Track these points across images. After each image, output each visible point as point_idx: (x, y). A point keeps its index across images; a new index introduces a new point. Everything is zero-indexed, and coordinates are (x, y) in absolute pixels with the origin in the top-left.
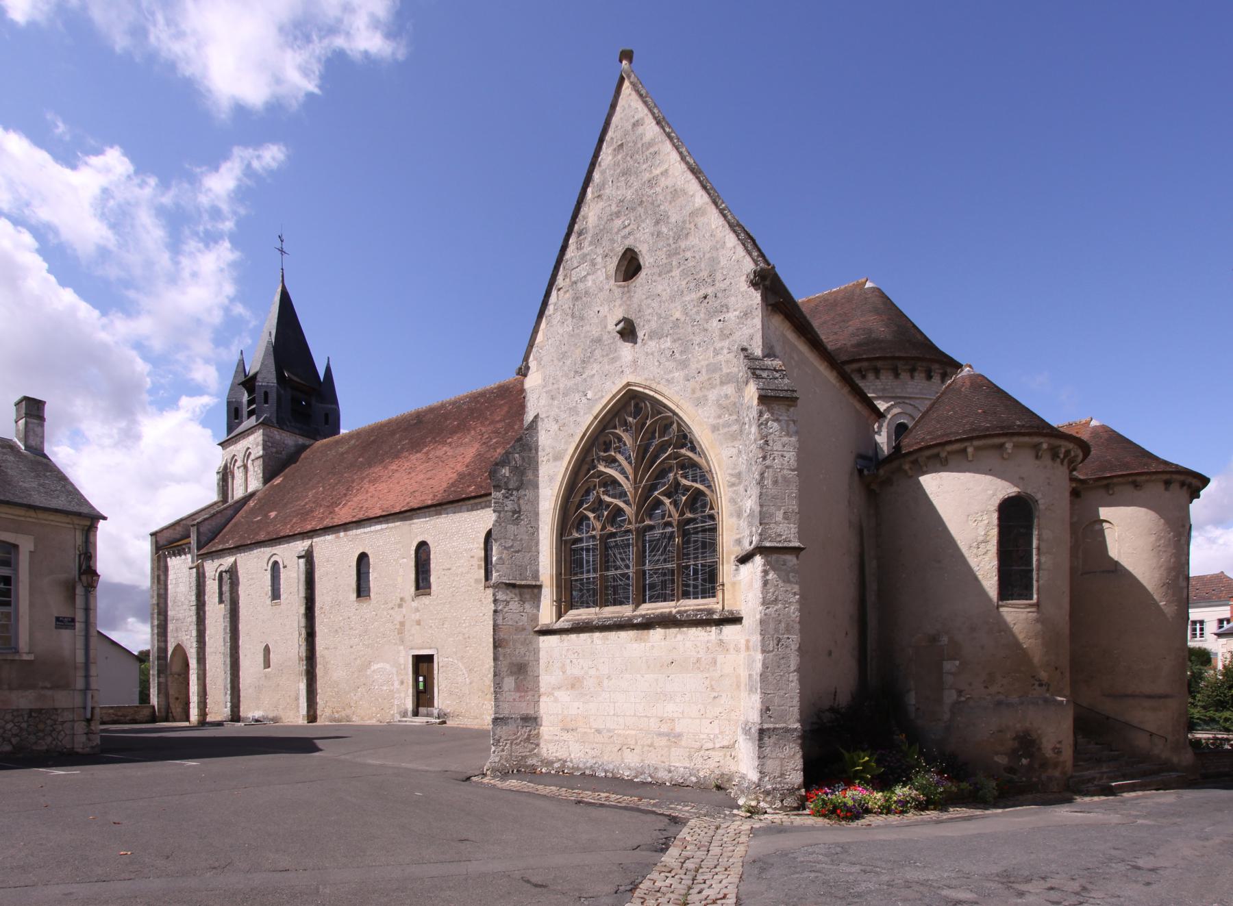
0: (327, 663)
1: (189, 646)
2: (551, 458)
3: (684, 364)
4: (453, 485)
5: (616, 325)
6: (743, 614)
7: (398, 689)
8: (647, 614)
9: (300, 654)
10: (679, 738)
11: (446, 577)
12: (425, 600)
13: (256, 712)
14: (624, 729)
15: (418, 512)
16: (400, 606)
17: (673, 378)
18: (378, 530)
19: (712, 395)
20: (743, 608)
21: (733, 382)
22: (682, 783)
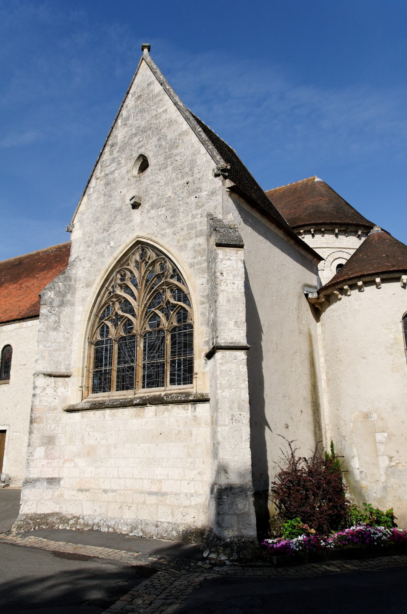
2: (84, 286)
3: (173, 225)
5: (131, 200)
6: (210, 396)
8: (144, 397)
10: (164, 497)
17: (165, 233)
19: (190, 244)
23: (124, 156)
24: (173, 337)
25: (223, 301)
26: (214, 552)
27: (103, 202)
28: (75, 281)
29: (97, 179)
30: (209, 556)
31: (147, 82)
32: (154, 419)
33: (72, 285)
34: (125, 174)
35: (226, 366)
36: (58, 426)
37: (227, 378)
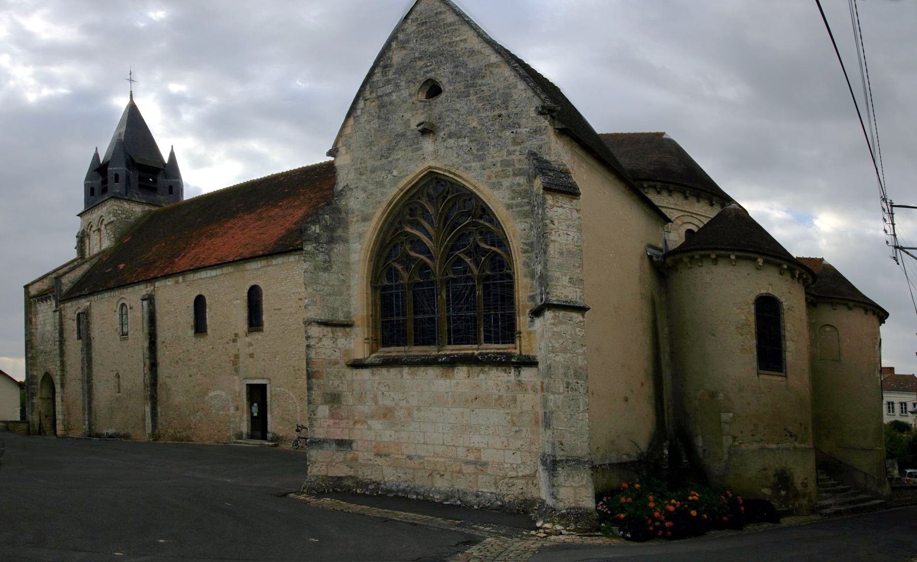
0: (169, 390)
1: (55, 373)
2: (360, 219)
3: (481, 158)
4: (280, 239)
5: (418, 126)
6: (539, 359)
7: (233, 414)
8: (451, 354)
9: (146, 381)
10: (485, 467)
11: (277, 316)
12: (257, 336)
13: (110, 429)
14: (433, 457)
15: (250, 260)
16: (234, 341)
17: (470, 167)
18: (214, 276)
19: (506, 182)
20: (538, 354)
21: (524, 175)
22: (489, 506)
23: (403, 78)
24: (486, 287)
25: (554, 253)
26: (548, 522)
27: (377, 125)
28: (347, 213)
29: (366, 100)
30: (544, 526)
31: (435, 11)
32: (466, 381)
33: (343, 218)
34: (408, 98)
35: (559, 328)
36: (342, 383)
37: (561, 341)
